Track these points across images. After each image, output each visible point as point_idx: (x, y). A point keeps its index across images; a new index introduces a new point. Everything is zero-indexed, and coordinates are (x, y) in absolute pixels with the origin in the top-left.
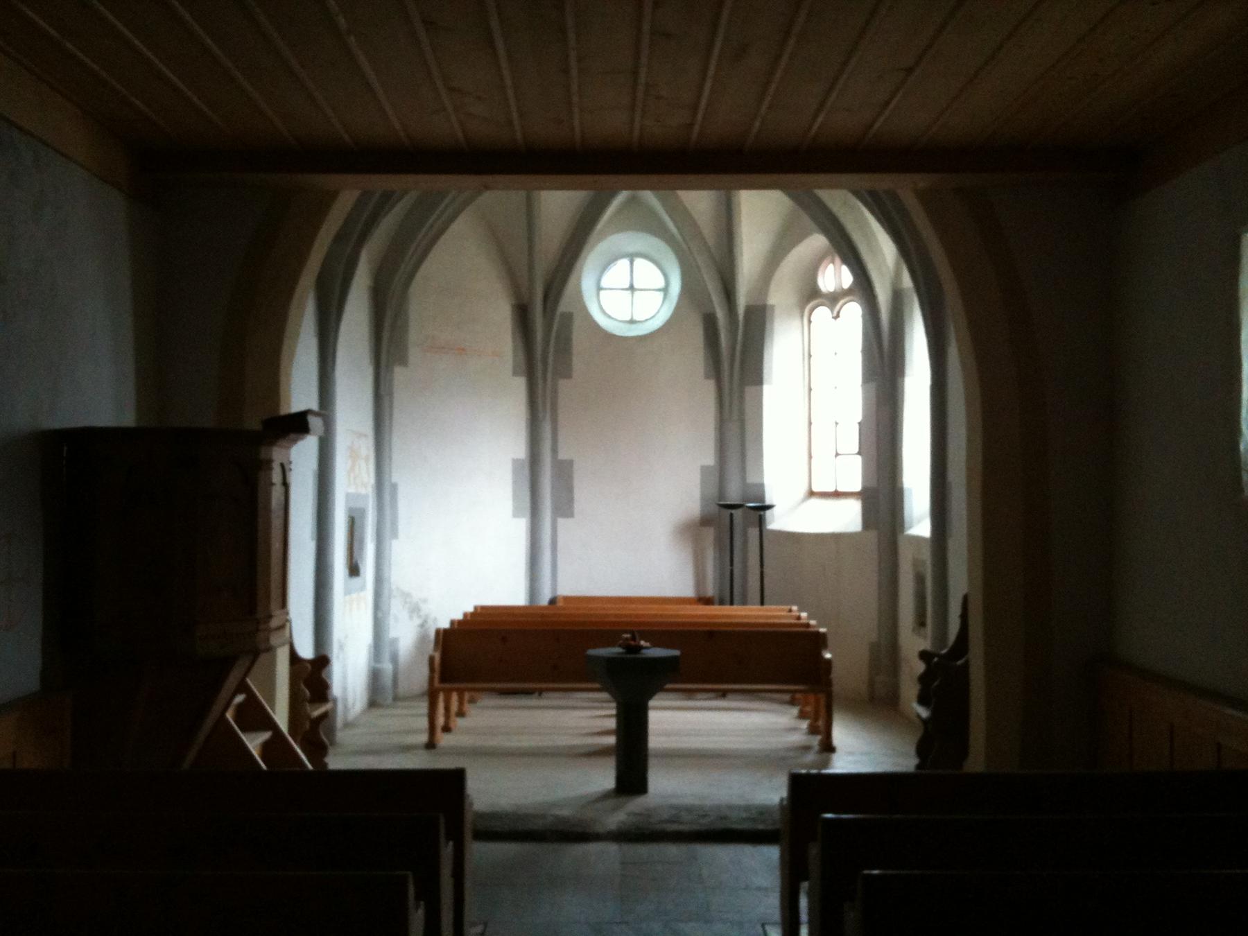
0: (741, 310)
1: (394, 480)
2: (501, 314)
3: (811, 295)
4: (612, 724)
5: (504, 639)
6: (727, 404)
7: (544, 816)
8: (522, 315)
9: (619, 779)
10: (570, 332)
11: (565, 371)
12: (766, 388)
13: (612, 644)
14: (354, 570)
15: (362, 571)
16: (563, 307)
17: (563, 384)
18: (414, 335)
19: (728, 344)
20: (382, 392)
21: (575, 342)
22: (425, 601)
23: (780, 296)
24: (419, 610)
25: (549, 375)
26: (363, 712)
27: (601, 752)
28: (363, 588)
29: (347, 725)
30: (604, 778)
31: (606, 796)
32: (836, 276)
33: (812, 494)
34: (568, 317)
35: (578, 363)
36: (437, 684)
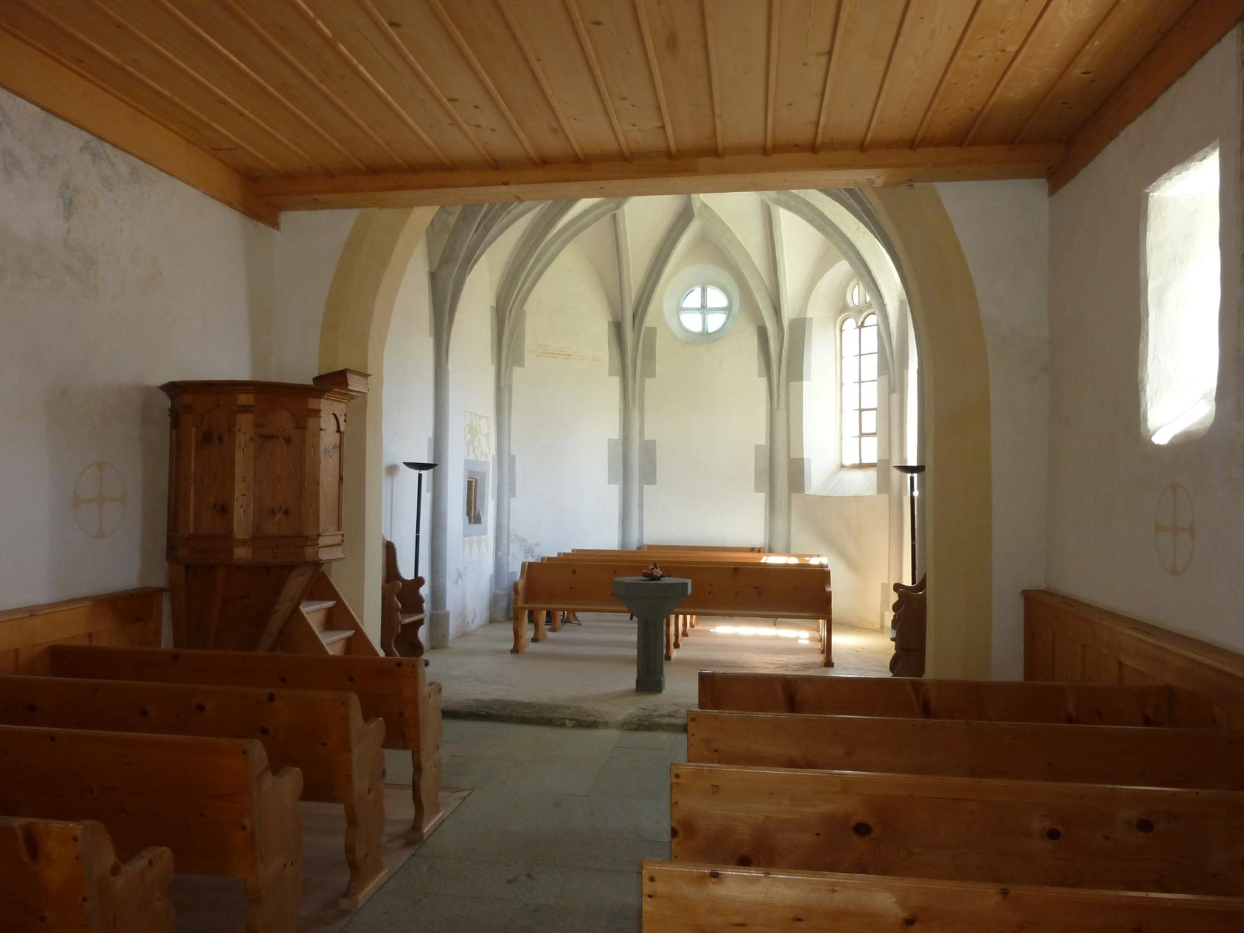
0: (786, 324)
1: (513, 452)
2: (600, 327)
3: (843, 309)
4: (634, 638)
5: (574, 572)
6: (775, 397)
7: (569, 707)
8: (617, 328)
9: (639, 682)
10: (321, 208)
11: (650, 372)
12: (806, 384)
13: (637, 575)
14: (473, 515)
15: (483, 520)
16: (649, 322)
17: (648, 382)
18: (530, 343)
19: (781, 354)
20: (503, 385)
21: (313, 212)
22: (537, 545)
23: (817, 312)
24: (533, 551)
25: (638, 375)
26: (483, 626)
27: (624, 660)
28: (484, 532)
29: (464, 635)
30: (629, 679)
31: (625, 695)
32: (857, 295)
33: (842, 466)
34: (652, 331)
35: (659, 367)
36: (520, 604)
